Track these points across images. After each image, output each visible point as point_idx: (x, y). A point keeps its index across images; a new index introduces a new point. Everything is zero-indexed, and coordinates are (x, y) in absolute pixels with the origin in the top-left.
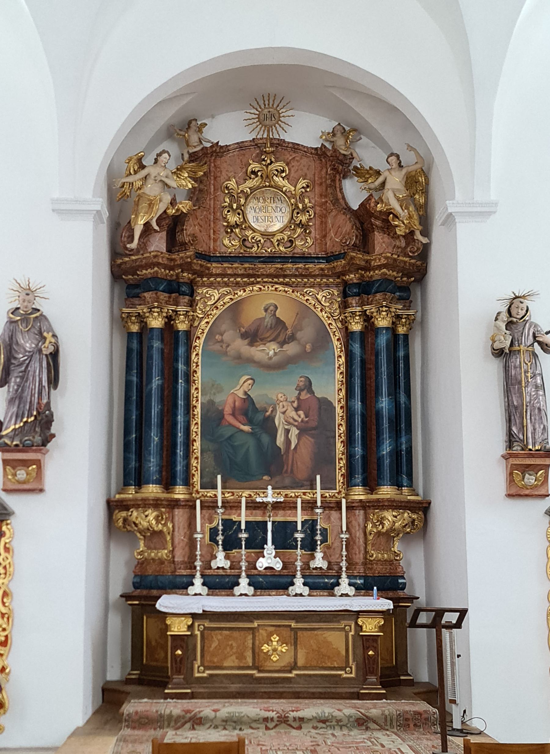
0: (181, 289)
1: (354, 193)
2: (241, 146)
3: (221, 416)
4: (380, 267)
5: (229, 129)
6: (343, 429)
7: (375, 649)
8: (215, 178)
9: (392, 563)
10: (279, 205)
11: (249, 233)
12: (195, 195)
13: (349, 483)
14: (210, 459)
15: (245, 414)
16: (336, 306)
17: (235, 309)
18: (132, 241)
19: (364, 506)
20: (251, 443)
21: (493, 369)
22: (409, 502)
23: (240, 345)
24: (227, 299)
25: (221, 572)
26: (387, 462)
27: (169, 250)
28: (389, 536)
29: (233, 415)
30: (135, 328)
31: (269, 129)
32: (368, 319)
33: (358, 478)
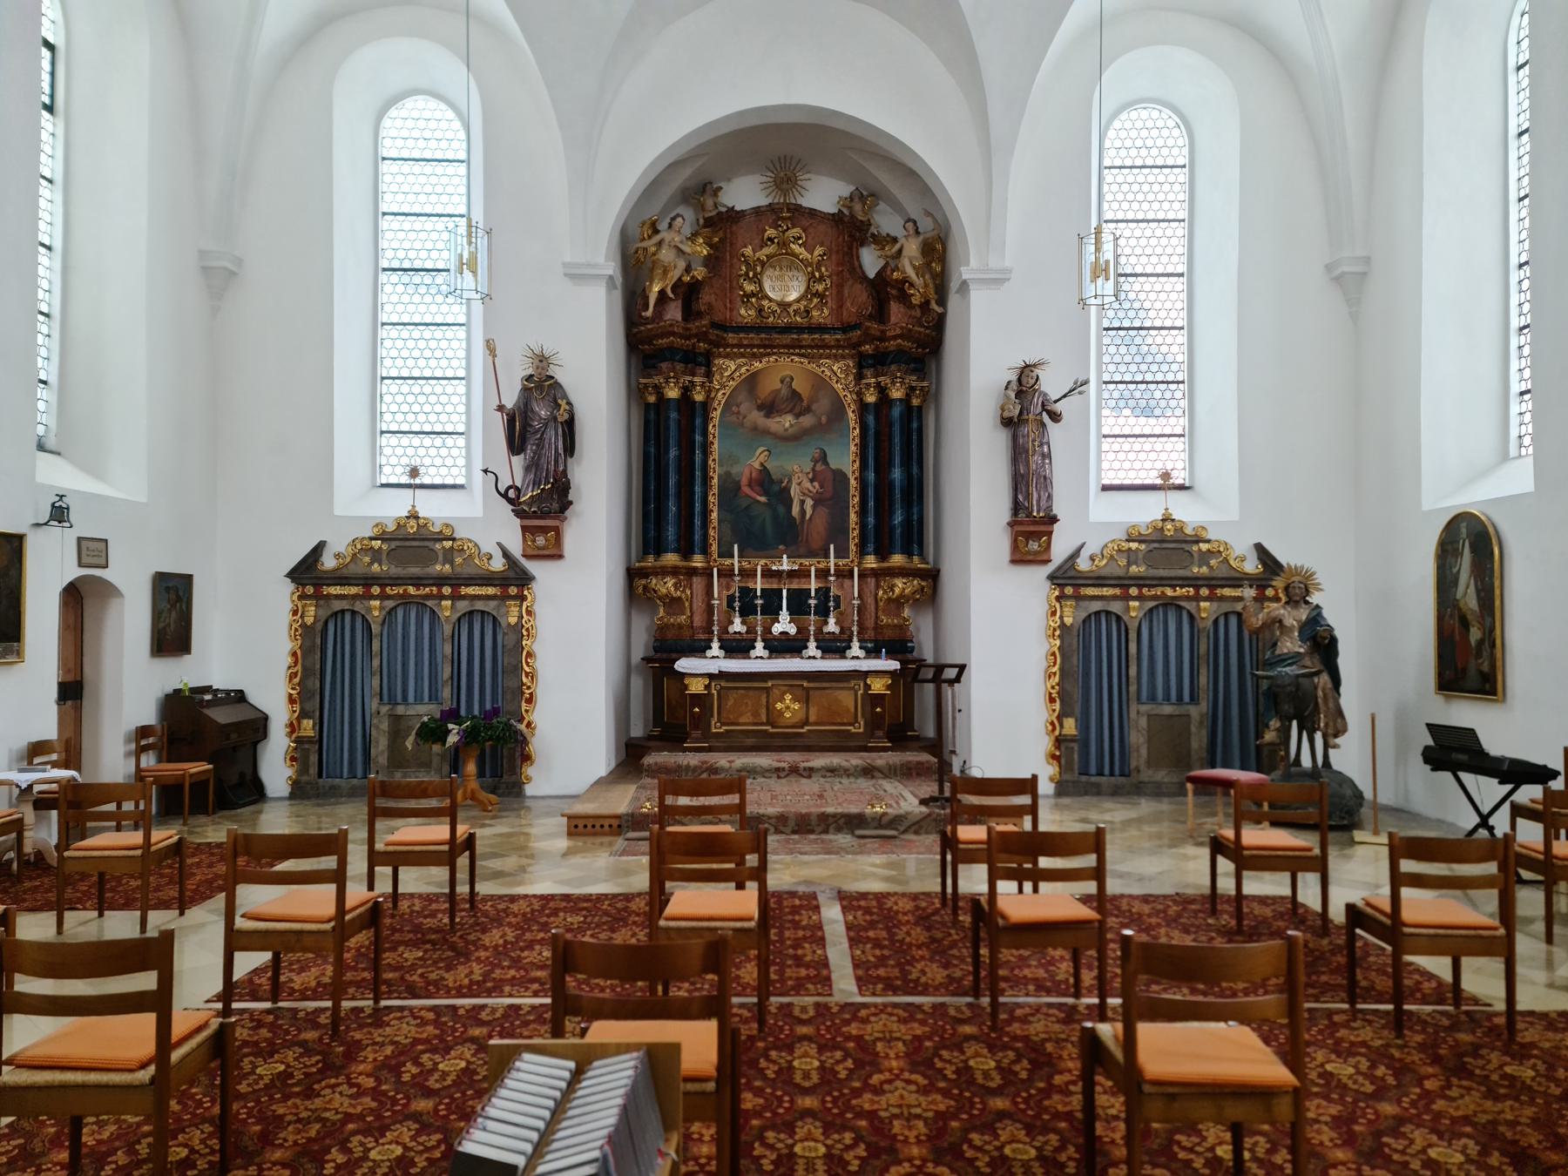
0: (699, 361)
1: (870, 261)
2: (757, 211)
3: (738, 487)
4: (895, 338)
6: (856, 500)
9: (902, 628)
11: (765, 303)
12: (711, 262)
13: (862, 552)
16: (851, 378)
17: (752, 380)
19: (877, 574)
20: (767, 515)
21: (1002, 438)
23: (756, 417)
27: (686, 318)
28: (898, 603)
29: (750, 485)
30: (652, 399)
31: (785, 193)
33: (871, 547)
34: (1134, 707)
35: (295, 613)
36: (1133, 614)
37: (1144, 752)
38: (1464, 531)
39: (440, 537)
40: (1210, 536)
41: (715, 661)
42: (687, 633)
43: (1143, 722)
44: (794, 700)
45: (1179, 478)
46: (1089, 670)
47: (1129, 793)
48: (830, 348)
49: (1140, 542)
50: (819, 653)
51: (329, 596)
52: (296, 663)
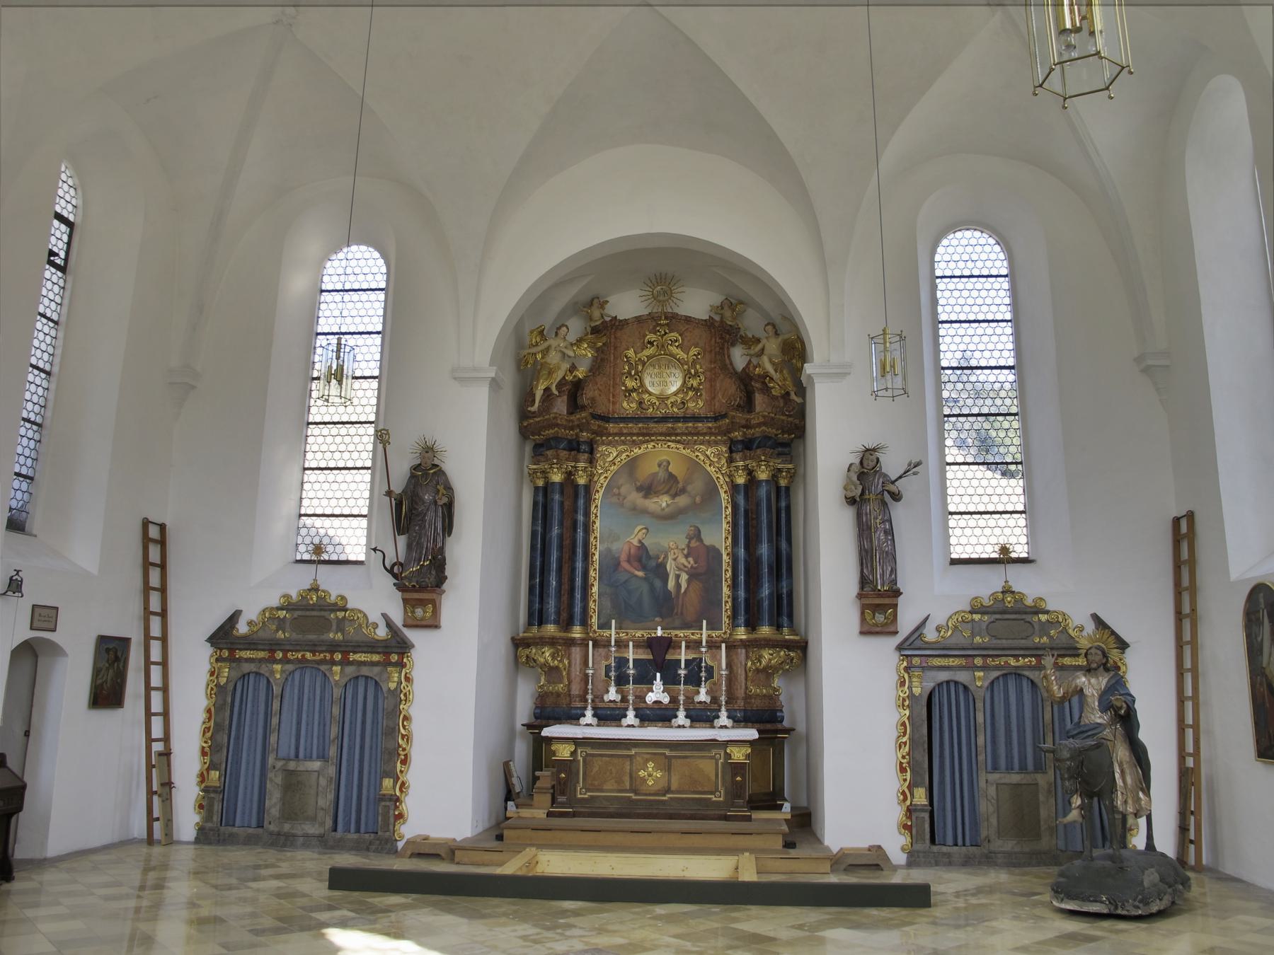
0: (585, 448)
1: (739, 358)
2: (639, 320)
3: (617, 564)
4: (759, 425)
5: (627, 304)
6: (729, 574)
7: (743, 776)
8: (615, 348)
9: (773, 698)
10: (673, 370)
11: (646, 396)
12: (597, 366)
13: (734, 624)
14: (607, 603)
15: (639, 560)
16: (723, 461)
17: (632, 464)
18: (533, 405)
19: (746, 644)
20: (645, 588)
21: (848, 514)
22: (786, 641)
23: (636, 498)
24: (624, 456)
25: (612, 705)
26: (766, 603)
27: (570, 413)
28: (767, 673)
29: (629, 561)
30: (541, 483)
31: (663, 303)
32: (750, 473)
33: (742, 619)
34: (983, 777)
35: (212, 674)
36: (979, 684)
37: (994, 821)
38: (1262, 600)
39: (335, 608)
40: (1049, 608)
41: (588, 727)
42: (564, 702)
43: (992, 791)
44: (656, 768)
45: (1020, 551)
46: (935, 735)
47: (980, 863)
48: (705, 434)
49: (983, 613)
50: (688, 723)
51: (240, 660)
52: (209, 719)
